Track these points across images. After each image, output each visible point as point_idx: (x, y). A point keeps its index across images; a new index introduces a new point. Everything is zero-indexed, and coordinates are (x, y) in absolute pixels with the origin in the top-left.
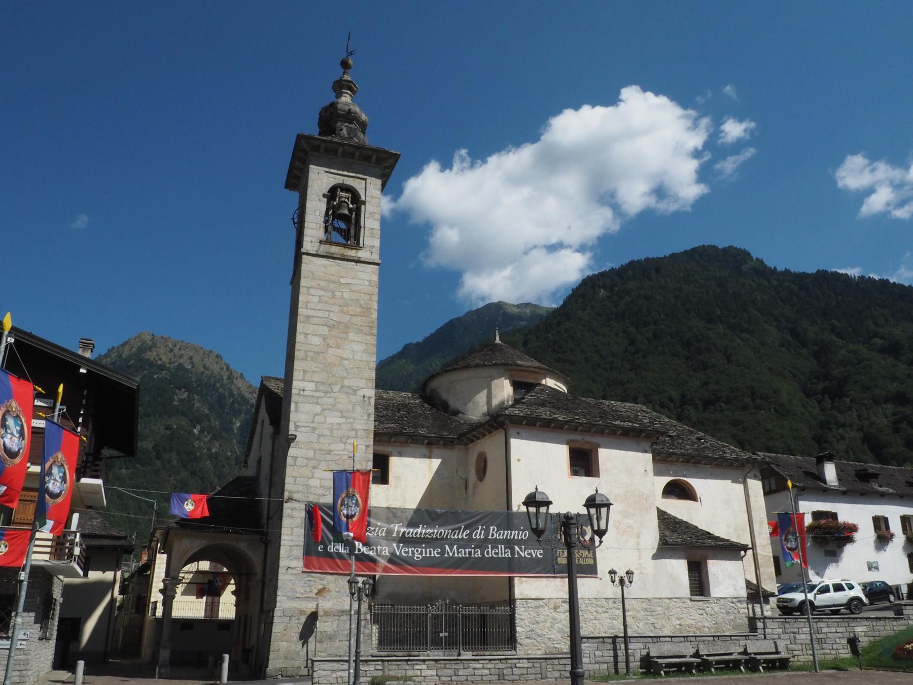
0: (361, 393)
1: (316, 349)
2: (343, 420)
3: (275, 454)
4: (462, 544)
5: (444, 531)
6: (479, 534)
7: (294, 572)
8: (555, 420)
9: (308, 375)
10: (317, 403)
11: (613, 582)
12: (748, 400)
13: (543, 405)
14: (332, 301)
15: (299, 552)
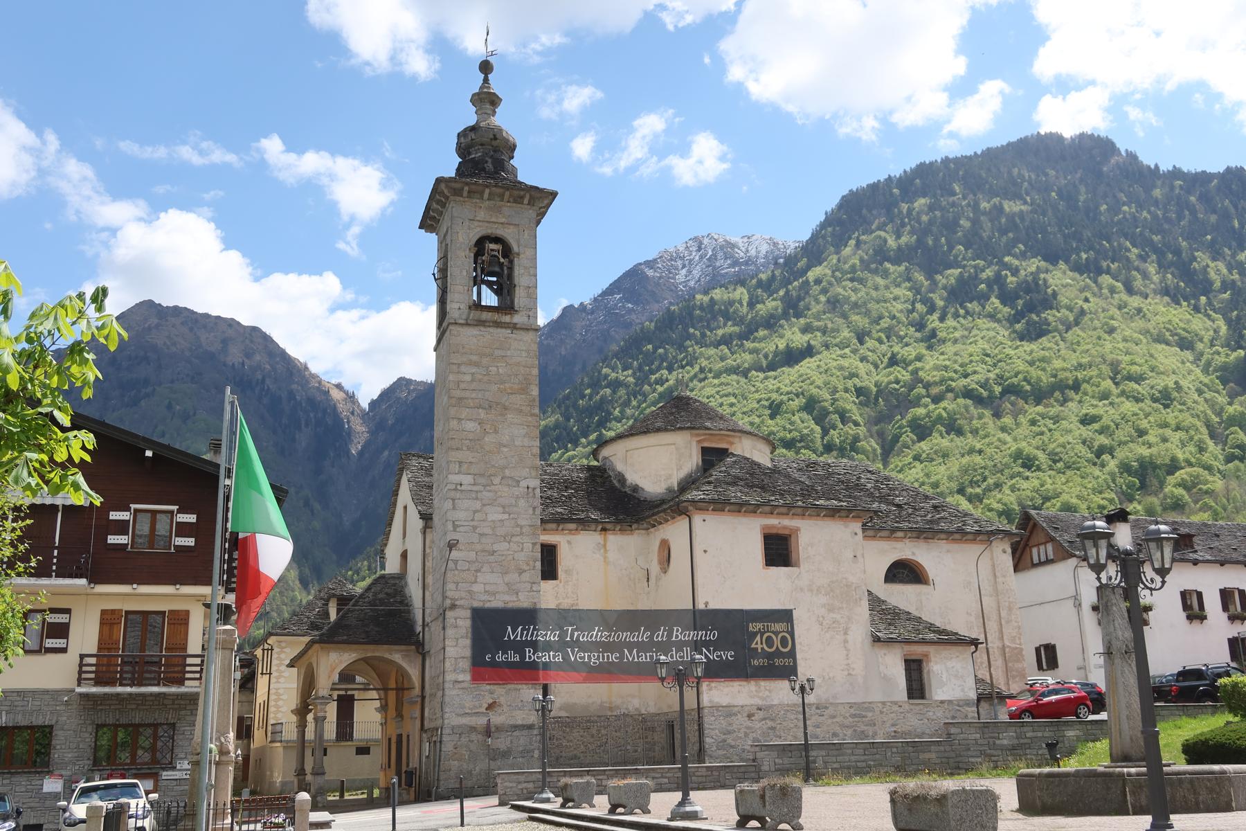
0: (524, 484)
1: (471, 436)
2: (506, 516)
3: (428, 551)
4: (641, 647)
5: (625, 636)
6: (661, 635)
7: (463, 685)
8: (747, 503)
9: (465, 466)
10: (477, 499)
11: (793, 689)
12: (1107, 384)
13: (734, 484)
14: (486, 378)
15: (466, 664)
